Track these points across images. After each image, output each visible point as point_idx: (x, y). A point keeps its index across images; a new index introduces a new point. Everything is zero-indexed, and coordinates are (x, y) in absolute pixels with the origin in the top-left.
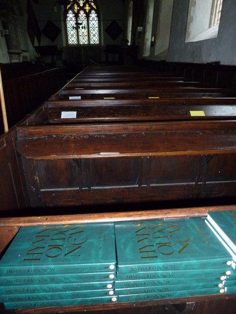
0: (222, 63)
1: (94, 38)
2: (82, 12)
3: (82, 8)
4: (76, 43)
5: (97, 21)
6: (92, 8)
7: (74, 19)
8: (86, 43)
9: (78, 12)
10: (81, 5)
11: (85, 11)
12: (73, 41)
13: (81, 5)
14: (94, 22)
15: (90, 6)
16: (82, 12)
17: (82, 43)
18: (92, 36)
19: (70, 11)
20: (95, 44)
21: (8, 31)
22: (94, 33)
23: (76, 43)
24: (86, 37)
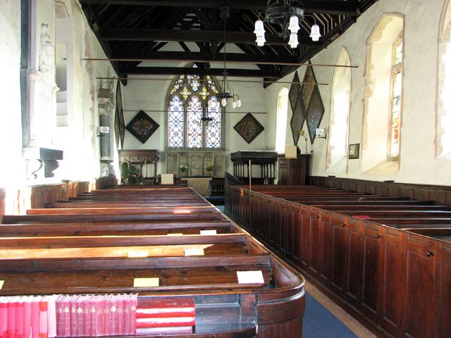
0: (395, 182)
1: (176, 139)
2: (195, 100)
3: (194, 93)
4: (181, 145)
5: (219, 114)
6: (212, 94)
7: (180, 109)
8: (198, 146)
9: (189, 98)
10: (195, 89)
11: (181, 98)
12: (176, 143)
13: (195, 89)
14: (176, 114)
15: (209, 90)
16: (195, 100)
17: (191, 146)
18: (209, 136)
19: (176, 98)
20: (175, 148)
21: (108, 128)
22: (176, 130)
23: (181, 145)
24: (190, 133)
